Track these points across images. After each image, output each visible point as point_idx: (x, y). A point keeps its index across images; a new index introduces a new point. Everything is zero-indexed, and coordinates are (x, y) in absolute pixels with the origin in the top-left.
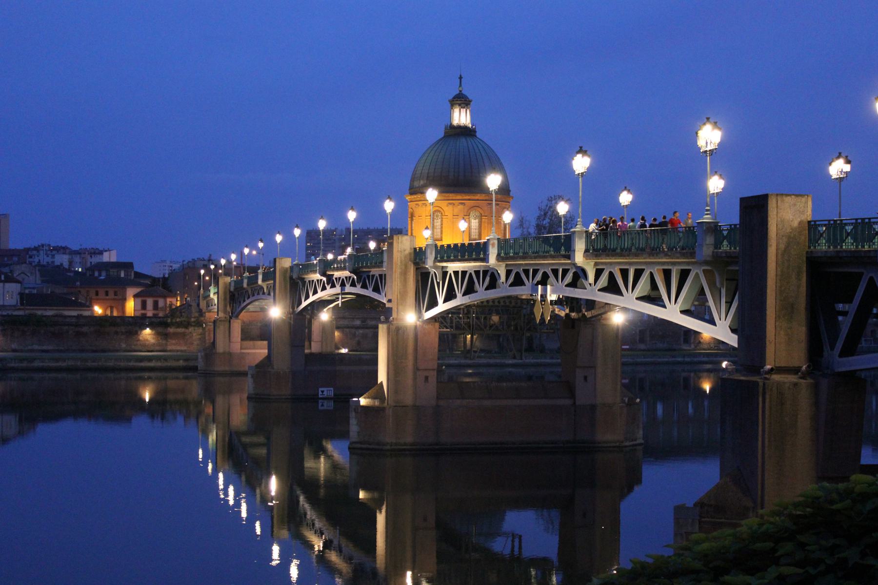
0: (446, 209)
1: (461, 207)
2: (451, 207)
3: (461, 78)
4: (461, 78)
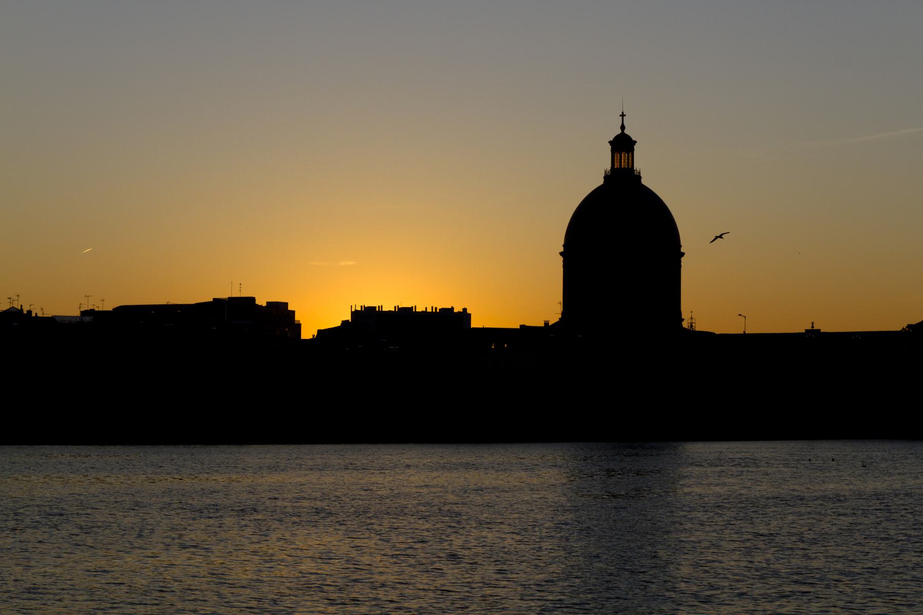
4: (623, 115)
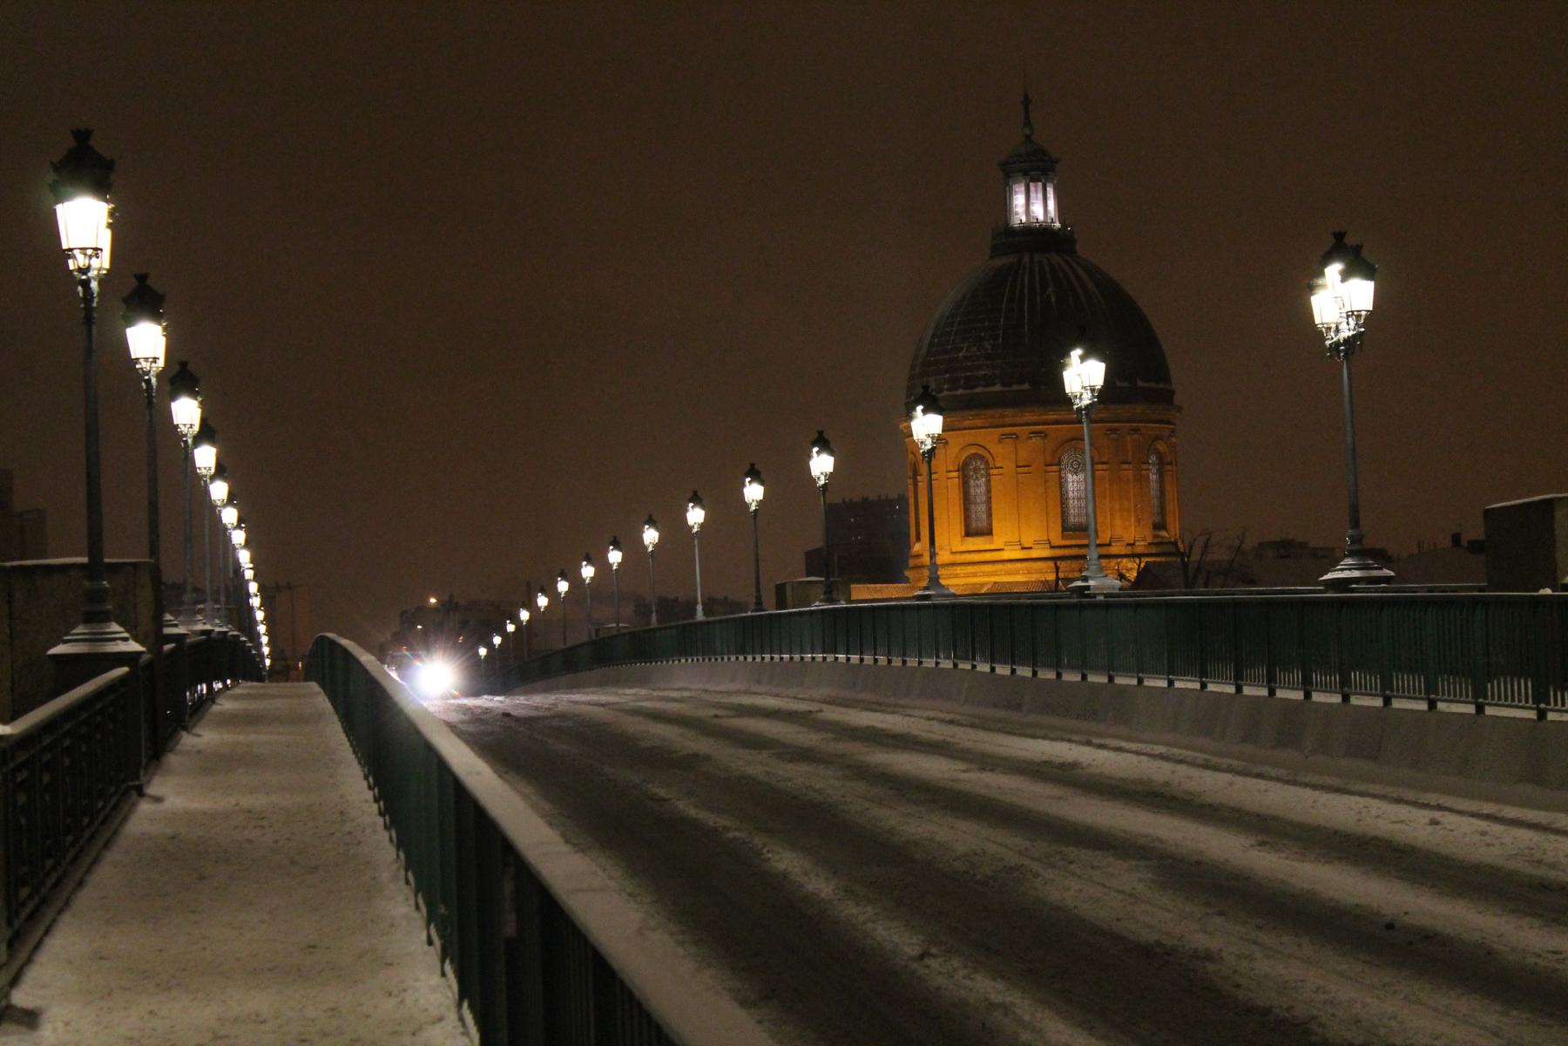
0: (996, 449)
1: (1036, 441)
2: (1008, 446)
3: (1027, 102)
4: (1027, 102)
